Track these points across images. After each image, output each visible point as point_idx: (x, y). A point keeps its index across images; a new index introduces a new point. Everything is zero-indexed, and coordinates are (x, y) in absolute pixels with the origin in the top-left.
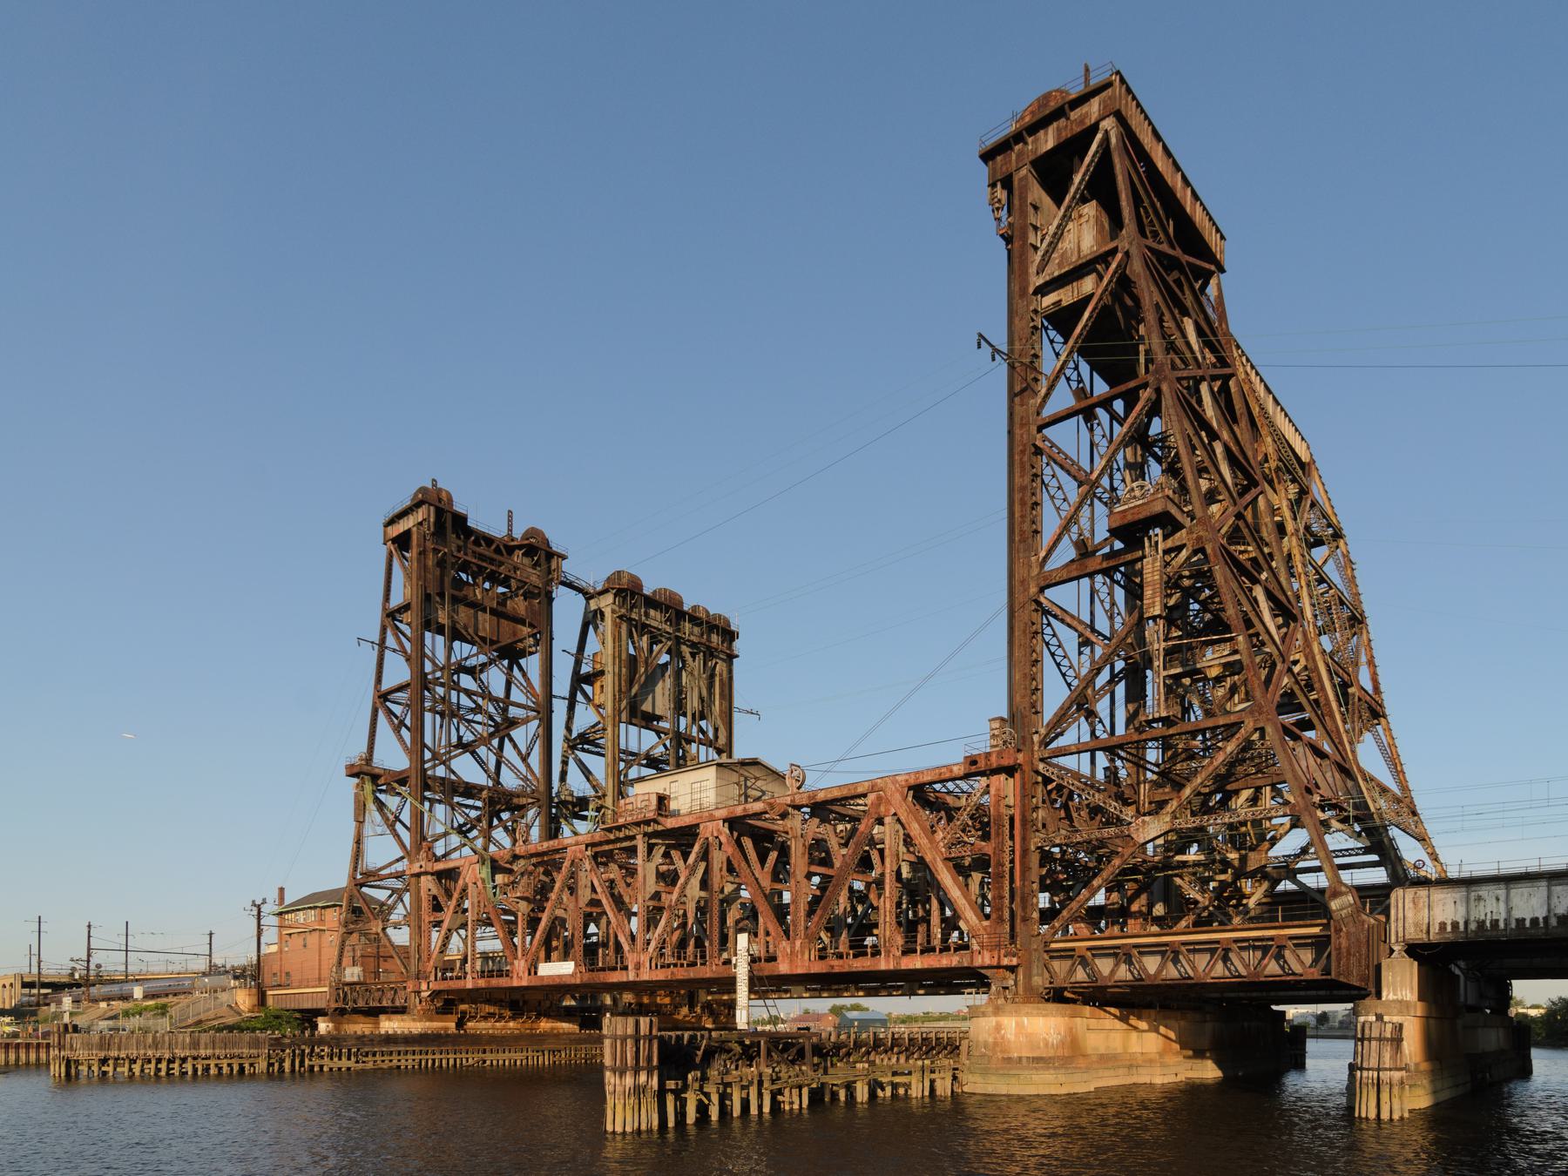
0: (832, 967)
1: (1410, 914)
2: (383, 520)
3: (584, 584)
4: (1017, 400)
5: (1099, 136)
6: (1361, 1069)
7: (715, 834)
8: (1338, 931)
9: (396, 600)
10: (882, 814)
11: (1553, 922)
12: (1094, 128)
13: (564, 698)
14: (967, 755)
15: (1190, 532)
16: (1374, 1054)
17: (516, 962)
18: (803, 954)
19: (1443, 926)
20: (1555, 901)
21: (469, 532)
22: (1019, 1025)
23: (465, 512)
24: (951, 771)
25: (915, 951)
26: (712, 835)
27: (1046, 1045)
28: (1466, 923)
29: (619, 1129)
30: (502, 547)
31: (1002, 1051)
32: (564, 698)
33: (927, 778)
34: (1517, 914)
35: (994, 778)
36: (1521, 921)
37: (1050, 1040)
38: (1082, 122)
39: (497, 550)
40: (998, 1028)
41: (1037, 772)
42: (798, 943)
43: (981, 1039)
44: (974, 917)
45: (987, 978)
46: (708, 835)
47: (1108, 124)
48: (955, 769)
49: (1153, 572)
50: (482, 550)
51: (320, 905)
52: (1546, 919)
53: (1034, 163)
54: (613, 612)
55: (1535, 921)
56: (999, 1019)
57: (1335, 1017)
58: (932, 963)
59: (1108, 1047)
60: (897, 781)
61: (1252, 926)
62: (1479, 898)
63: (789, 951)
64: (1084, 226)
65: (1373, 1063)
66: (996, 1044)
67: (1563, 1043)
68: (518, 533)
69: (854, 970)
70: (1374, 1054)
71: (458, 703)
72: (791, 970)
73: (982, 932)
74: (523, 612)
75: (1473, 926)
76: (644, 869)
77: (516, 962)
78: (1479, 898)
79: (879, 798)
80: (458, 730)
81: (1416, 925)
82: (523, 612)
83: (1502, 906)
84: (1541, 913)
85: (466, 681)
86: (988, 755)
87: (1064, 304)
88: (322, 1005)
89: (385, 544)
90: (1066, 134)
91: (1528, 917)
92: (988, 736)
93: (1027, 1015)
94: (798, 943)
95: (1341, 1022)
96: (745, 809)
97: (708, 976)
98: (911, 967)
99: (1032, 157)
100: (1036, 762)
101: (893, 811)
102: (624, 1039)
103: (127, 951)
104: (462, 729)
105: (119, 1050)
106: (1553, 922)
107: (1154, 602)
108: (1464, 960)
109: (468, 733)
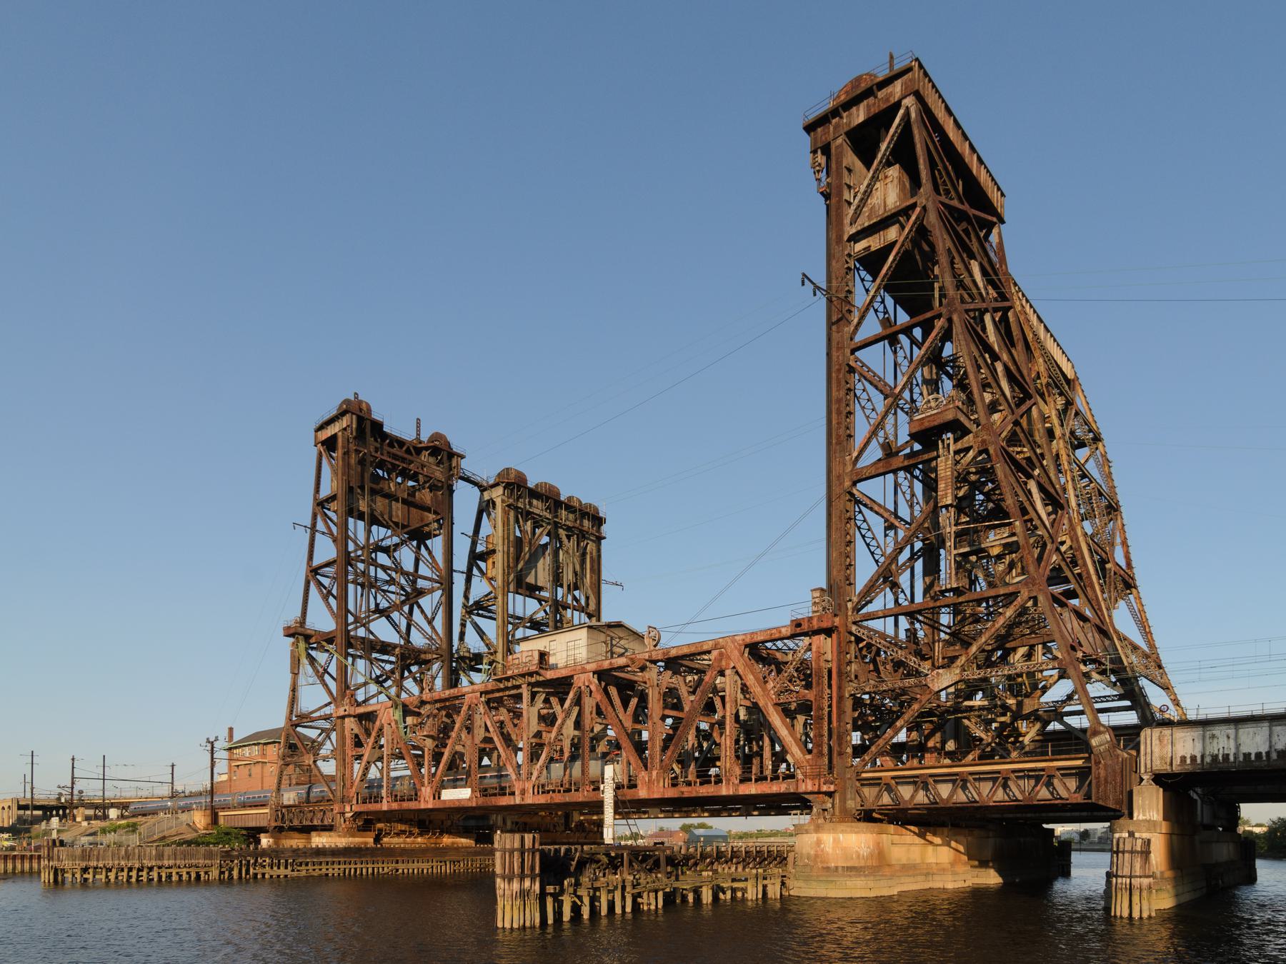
0: (683, 793)
2: (314, 426)
3: (479, 479)
5: (901, 112)
6: (1117, 876)
7: (587, 684)
8: (1098, 763)
9: (325, 492)
10: (723, 668)
11: (1274, 756)
12: (897, 105)
13: (462, 572)
14: (794, 619)
15: (976, 436)
16: (1127, 864)
18: (658, 782)
19: (1183, 759)
20: (1275, 738)
21: (385, 436)
22: (836, 841)
24: (780, 632)
25: (751, 780)
26: (584, 685)
27: (858, 856)
28: (1203, 757)
29: (507, 925)
31: (822, 862)
32: (462, 572)
33: (760, 638)
34: (1244, 749)
36: (1247, 755)
37: (861, 853)
38: (887, 100)
39: (408, 451)
40: (819, 842)
41: (851, 633)
42: (654, 773)
43: (804, 851)
44: (799, 752)
45: (810, 801)
46: (580, 684)
47: (909, 101)
49: (945, 469)
50: (395, 450)
52: (1268, 753)
53: (848, 134)
54: (503, 501)
55: (1259, 755)
56: (820, 835)
57: (1095, 834)
58: (765, 789)
59: (909, 859)
60: (735, 640)
61: (1027, 759)
62: (1213, 736)
63: (647, 779)
64: (889, 185)
65: (1126, 871)
66: (816, 856)
67: (1282, 855)
68: (425, 437)
69: (700, 795)
70: (1127, 864)
71: (376, 577)
73: (805, 764)
74: (429, 502)
75: (1208, 759)
76: (528, 712)
77: (423, 789)
78: (1213, 736)
79: (721, 654)
81: (1162, 758)
82: (429, 502)
83: (1232, 743)
84: (1264, 749)
85: (382, 558)
86: (810, 619)
87: (873, 249)
88: (264, 823)
89: (316, 446)
90: (875, 110)
91: (1253, 752)
92: (810, 604)
93: (842, 832)
94: (654, 773)
95: (1100, 838)
97: (580, 800)
99: (846, 129)
100: (850, 625)
101: (732, 665)
102: (512, 852)
103: (104, 779)
104: (379, 598)
106: (1274, 756)
107: (946, 494)
108: (1200, 787)
109: (384, 601)
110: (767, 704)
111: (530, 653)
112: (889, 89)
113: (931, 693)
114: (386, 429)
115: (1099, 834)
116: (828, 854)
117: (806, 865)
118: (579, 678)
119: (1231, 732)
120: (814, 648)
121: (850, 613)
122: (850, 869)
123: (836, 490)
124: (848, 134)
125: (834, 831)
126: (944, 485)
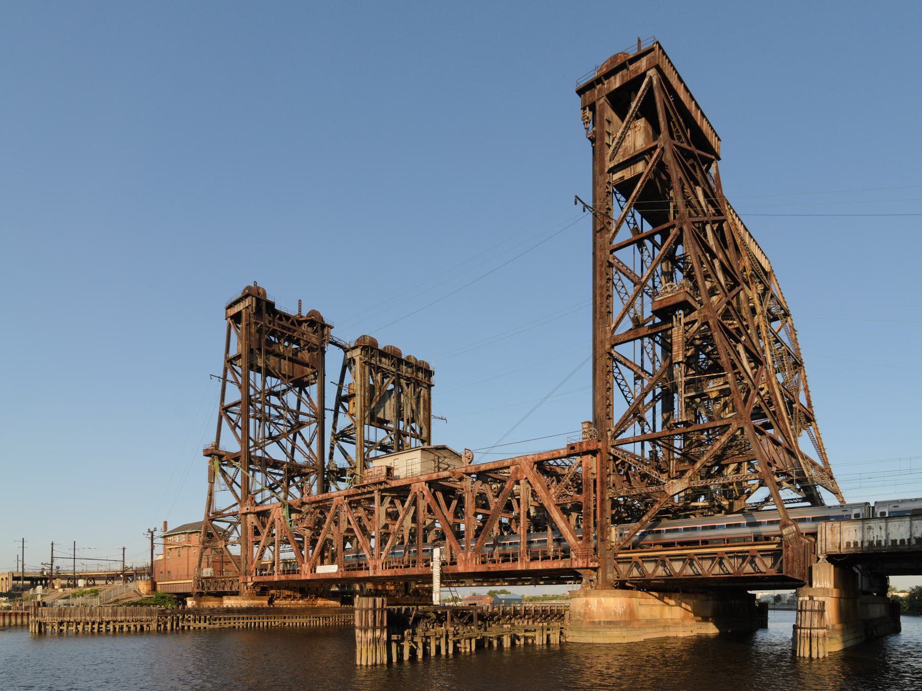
0: (489, 568)
1: (829, 537)
3: (343, 343)
4: (598, 235)
5: (646, 80)
6: (801, 628)
7: (421, 490)
8: (787, 547)
9: (233, 352)
10: (519, 479)
11: (913, 542)
12: (644, 75)
13: (332, 410)
14: (569, 443)
15: (700, 312)
16: (808, 620)
17: (303, 565)
18: (472, 561)
19: (848, 544)
20: (914, 529)
21: (276, 312)
22: (599, 603)
23: (273, 301)
24: (559, 453)
25: (538, 559)
26: (419, 491)
27: (615, 614)
28: (862, 542)
30: (295, 321)
31: (589, 618)
32: (332, 410)
33: (545, 457)
34: (892, 537)
35: (585, 457)
36: (894, 541)
38: (636, 71)
39: (293, 323)
40: (587, 604)
41: (610, 454)
43: (577, 610)
44: (573, 539)
45: (580, 574)
46: (416, 490)
47: (652, 73)
48: (562, 452)
50: (284, 323)
51: (188, 531)
52: (909, 540)
53: (607, 96)
54: (361, 359)
55: (902, 541)
56: (588, 598)
57: (785, 597)
60: (527, 459)
62: (870, 528)
64: (638, 133)
65: (808, 625)
66: (585, 613)
67: (919, 613)
68: (305, 313)
69: (502, 570)
70: (808, 620)
71: (269, 413)
72: (465, 570)
73: (577, 547)
74: (308, 360)
75: (866, 544)
76: (379, 511)
78: (870, 528)
79: (517, 469)
80: (269, 429)
81: (833, 543)
82: (308, 360)
84: (906, 537)
85: (274, 400)
86: (581, 444)
87: (626, 178)
88: (189, 590)
89: (226, 319)
90: (627, 79)
91: (898, 539)
93: (604, 596)
94: (469, 554)
95: (788, 601)
96: (438, 475)
97: (416, 573)
98: (536, 568)
99: (607, 92)
100: (609, 448)
101: (525, 477)
102: (367, 611)
105: (70, 617)
106: (913, 542)
107: (679, 354)
109: (275, 430)
110: (550, 505)
111: (380, 468)
112: (637, 64)
113: (667, 496)
114: (276, 307)
115: (788, 598)
116: (593, 612)
117: (578, 620)
118: (415, 486)
119: (883, 524)
120: (584, 464)
121: (609, 439)
122: (610, 623)
123: (600, 351)
124: (607, 96)
125: (598, 595)
126: (676, 348)
